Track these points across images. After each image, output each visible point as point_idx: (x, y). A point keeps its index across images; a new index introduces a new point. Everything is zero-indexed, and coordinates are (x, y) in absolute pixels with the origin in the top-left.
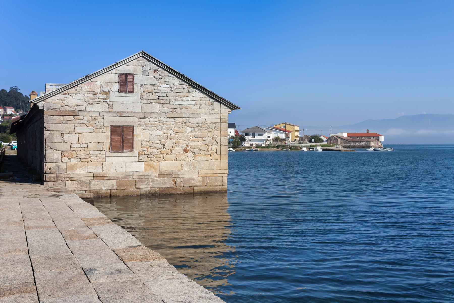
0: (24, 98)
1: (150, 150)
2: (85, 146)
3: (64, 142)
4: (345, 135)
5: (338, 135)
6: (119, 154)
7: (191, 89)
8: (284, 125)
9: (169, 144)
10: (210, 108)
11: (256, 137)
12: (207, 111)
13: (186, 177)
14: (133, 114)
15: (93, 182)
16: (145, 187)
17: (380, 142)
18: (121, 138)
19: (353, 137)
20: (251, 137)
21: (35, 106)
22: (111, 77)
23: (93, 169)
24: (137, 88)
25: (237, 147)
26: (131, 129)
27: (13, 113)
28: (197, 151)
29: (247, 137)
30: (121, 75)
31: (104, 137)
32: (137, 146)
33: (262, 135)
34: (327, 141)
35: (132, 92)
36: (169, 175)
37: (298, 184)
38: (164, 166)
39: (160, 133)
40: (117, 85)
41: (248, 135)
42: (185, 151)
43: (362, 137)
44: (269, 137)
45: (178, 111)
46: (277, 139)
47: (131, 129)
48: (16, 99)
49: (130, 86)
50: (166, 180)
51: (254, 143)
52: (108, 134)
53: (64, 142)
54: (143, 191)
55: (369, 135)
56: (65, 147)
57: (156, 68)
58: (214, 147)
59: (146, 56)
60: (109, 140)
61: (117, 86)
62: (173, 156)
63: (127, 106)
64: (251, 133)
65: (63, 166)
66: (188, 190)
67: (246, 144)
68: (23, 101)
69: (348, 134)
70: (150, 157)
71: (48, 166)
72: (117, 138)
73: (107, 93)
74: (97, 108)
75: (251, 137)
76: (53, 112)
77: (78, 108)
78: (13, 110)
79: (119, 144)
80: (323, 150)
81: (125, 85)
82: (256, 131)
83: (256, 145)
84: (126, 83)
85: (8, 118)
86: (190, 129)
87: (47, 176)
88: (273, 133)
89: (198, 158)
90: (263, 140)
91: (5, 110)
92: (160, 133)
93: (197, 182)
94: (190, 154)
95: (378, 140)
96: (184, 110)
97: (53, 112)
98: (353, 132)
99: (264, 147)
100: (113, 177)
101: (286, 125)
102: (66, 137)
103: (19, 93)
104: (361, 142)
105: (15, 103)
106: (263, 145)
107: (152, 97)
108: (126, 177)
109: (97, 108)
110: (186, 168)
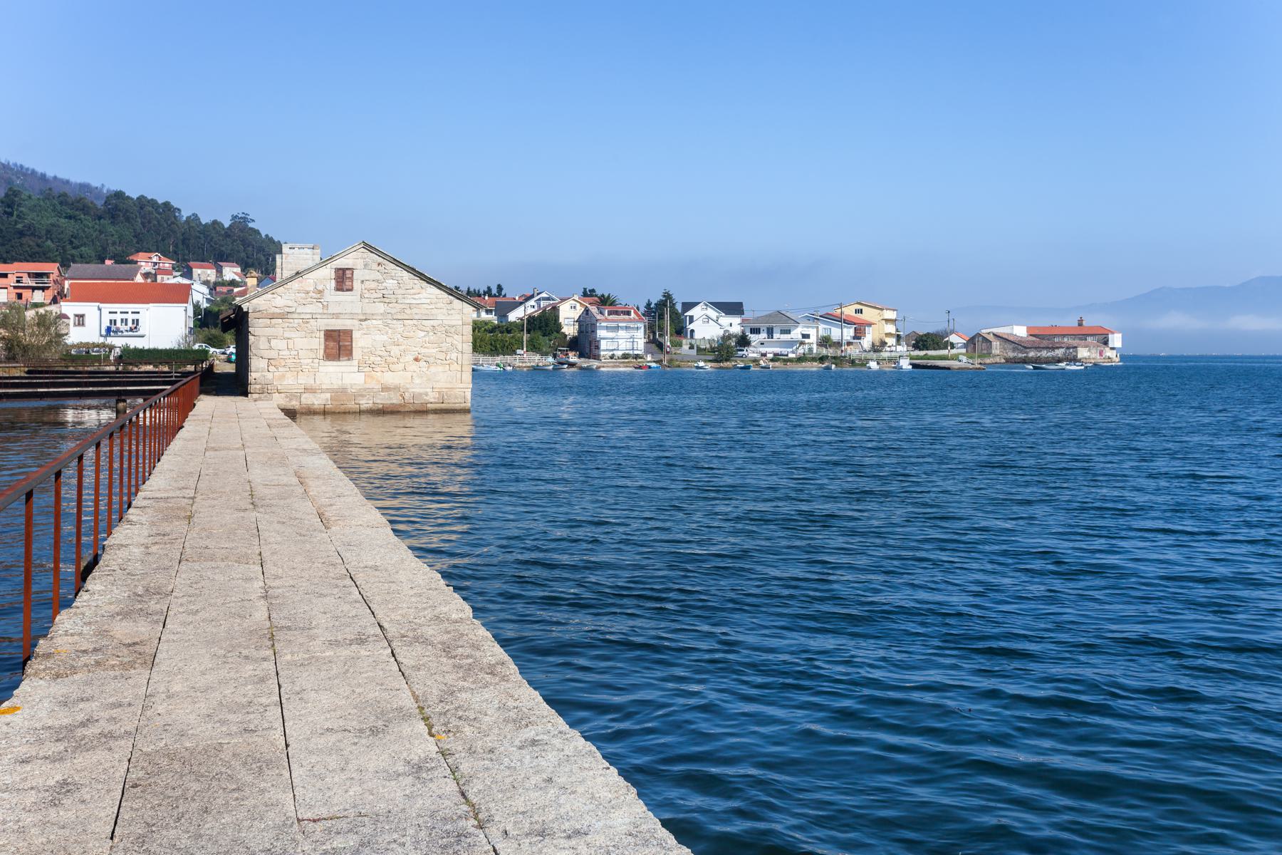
0: (263, 241)
1: (372, 358)
2: (294, 353)
3: (271, 348)
4: (1020, 331)
5: (995, 330)
6: (335, 363)
7: (424, 284)
8: (859, 307)
9: (395, 351)
10: (449, 307)
11: (776, 336)
12: (445, 311)
13: (417, 391)
14: (352, 316)
15: (304, 396)
16: (366, 403)
17: (1113, 349)
18: (338, 344)
19: (1043, 338)
20: (763, 335)
21: (240, 308)
22: (328, 273)
23: (305, 380)
24: (357, 285)
25: (727, 360)
26: (348, 333)
27: (238, 279)
28: (431, 360)
29: (754, 338)
30: (337, 270)
31: (318, 343)
32: (357, 353)
33: (788, 332)
34: (965, 346)
35: (351, 290)
36: (397, 388)
37: (921, 460)
38: (390, 378)
39: (385, 338)
40: (333, 282)
41: (756, 331)
42: (416, 360)
43: (1064, 336)
44: (806, 336)
45: (408, 311)
46: (825, 342)
47: (348, 333)
48: (245, 243)
49: (348, 283)
50: (392, 394)
51: (771, 351)
52: (322, 340)
53: (271, 348)
54: (363, 407)
55: (1082, 334)
56: (273, 354)
57: (380, 260)
58: (454, 356)
59: (368, 247)
60: (323, 347)
61: (333, 283)
62: (401, 366)
63: (344, 309)
64: (763, 327)
65: (270, 376)
66: (419, 408)
67: (751, 353)
68: (261, 250)
69: (1028, 329)
70: (372, 366)
71: (253, 376)
72: (332, 344)
73: (320, 292)
74: (309, 309)
75: (763, 335)
76: (257, 315)
77: (288, 310)
78: (238, 270)
79: (335, 351)
80: (915, 366)
81: (343, 282)
82: (776, 322)
83: (775, 355)
84: (343, 279)
85: (225, 289)
86: (423, 334)
87: (251, 388)
88: (821, 326)
89: (433, 369)
90: (790, 344)
91: (219, 271)
92: (385, 338)
93: (431, 398)
94: (422, 363)
95: (1106, 343)
96: (415, 311)
97: (257, 315)
98: (1044, 322)
99: (791, 360)
100: (327, 390)
101: (864, 308)
102: (273, 342)
103: (251, 229)
104: (1053, 349)
105: (243, 255)
106: (791, 356)
107: (375, 295)
108: (343, 390)
109: (309, 309)
110: (417, 381)
